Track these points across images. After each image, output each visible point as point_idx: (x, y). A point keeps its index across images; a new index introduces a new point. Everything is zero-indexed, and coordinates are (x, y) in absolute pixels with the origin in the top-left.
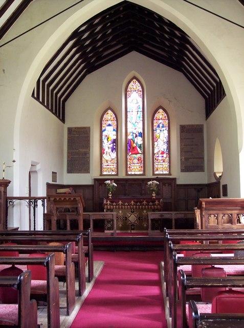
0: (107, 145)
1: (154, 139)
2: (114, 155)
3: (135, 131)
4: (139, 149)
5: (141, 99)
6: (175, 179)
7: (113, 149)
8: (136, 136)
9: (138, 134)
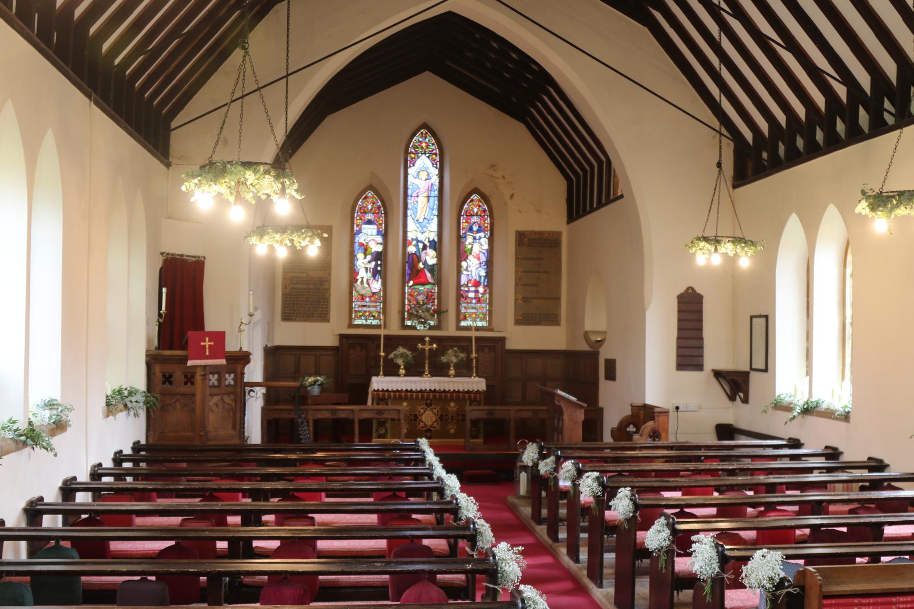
0: (363, 263)
1: (462, 254)
2: (377, 286)
3: (421, 237)
4: (428, 275)
5: (436, 171)
6: (502, 340)
7: (375, 273)
8: (425, 247)
9: (428, 244)
